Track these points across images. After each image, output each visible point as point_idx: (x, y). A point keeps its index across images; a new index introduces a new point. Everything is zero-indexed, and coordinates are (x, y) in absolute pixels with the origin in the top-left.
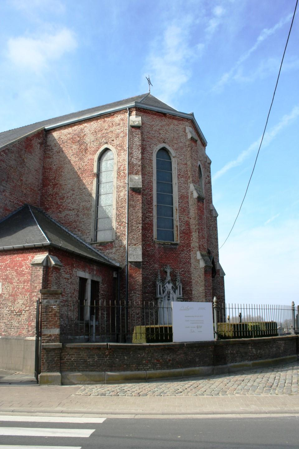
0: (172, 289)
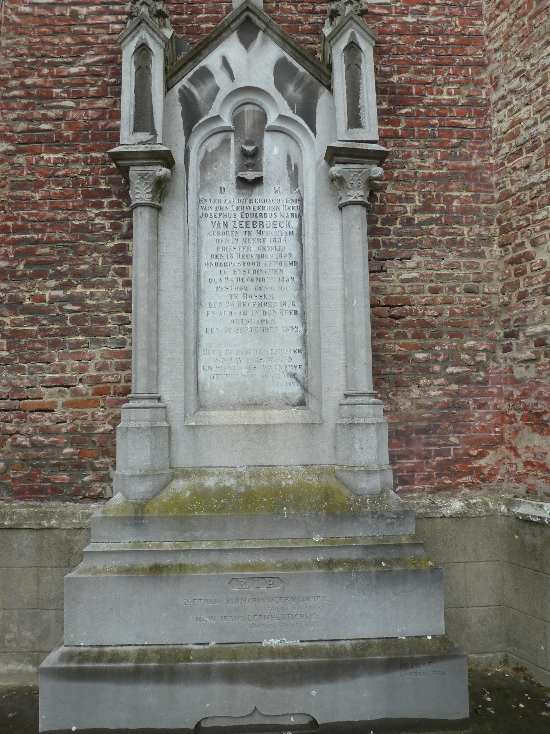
0: (280, 86)
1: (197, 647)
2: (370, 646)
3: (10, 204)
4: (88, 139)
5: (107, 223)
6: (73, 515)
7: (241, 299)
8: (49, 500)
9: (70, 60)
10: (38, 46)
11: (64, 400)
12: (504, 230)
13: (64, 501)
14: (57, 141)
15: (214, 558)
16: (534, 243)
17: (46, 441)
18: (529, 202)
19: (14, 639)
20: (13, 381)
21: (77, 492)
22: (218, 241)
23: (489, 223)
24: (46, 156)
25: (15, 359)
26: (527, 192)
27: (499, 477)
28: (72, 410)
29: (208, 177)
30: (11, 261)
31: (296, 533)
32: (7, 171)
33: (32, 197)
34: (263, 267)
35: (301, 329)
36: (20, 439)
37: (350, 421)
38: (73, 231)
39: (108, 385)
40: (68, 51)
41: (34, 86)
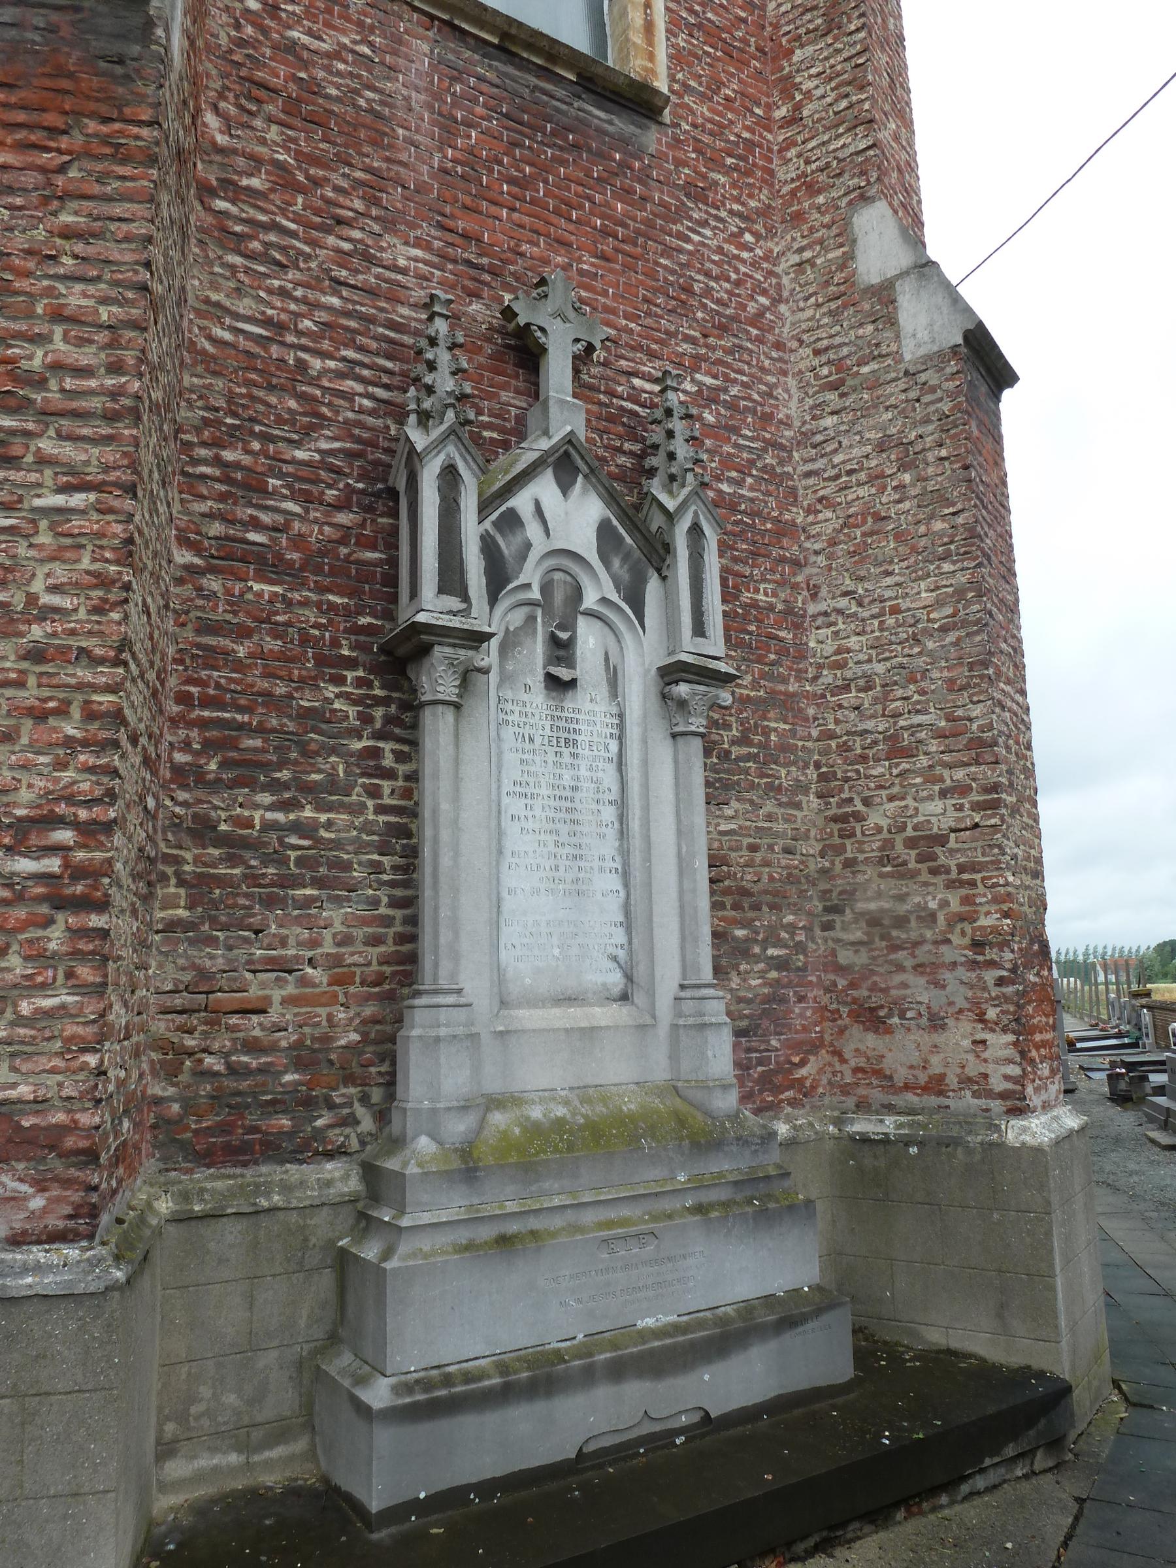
1: (563, 1345)
2: (753, 1308)
3: (193, 656)
4: (323, 570)
5: (352, 711)
6: (302, 1184)
7: (551, 848)
8: (256, 1163)
9: (295, 437)
10: (242, 402)
11: (284, 993)
12: (823, 777)
13: (282, 1162)
14: (274, 565)
15: (570, 1216)
16: (866, 802)
17: (254, 1064)
18: (859, 751)
19: (206, 1413)
20: (197, 961)
21: (305, 1146)
22: (522, 761)
23: (806, 766)
24: (257, 587)
25: (203, 924)
26: (858, 739)
27: (821, 1090)
28: (296, 1010)
29: (510, 667)
30: (197, 754)
31: (657, 1173)
32: (192, 600)
33: (233, 651)
34: (577, 805)
35: (622, 894)
36: (209, 1060)
37: (699, 1021)
38: (300, 716)
39: (353, 969)
40: (293, 422)
41: (237, 465)
